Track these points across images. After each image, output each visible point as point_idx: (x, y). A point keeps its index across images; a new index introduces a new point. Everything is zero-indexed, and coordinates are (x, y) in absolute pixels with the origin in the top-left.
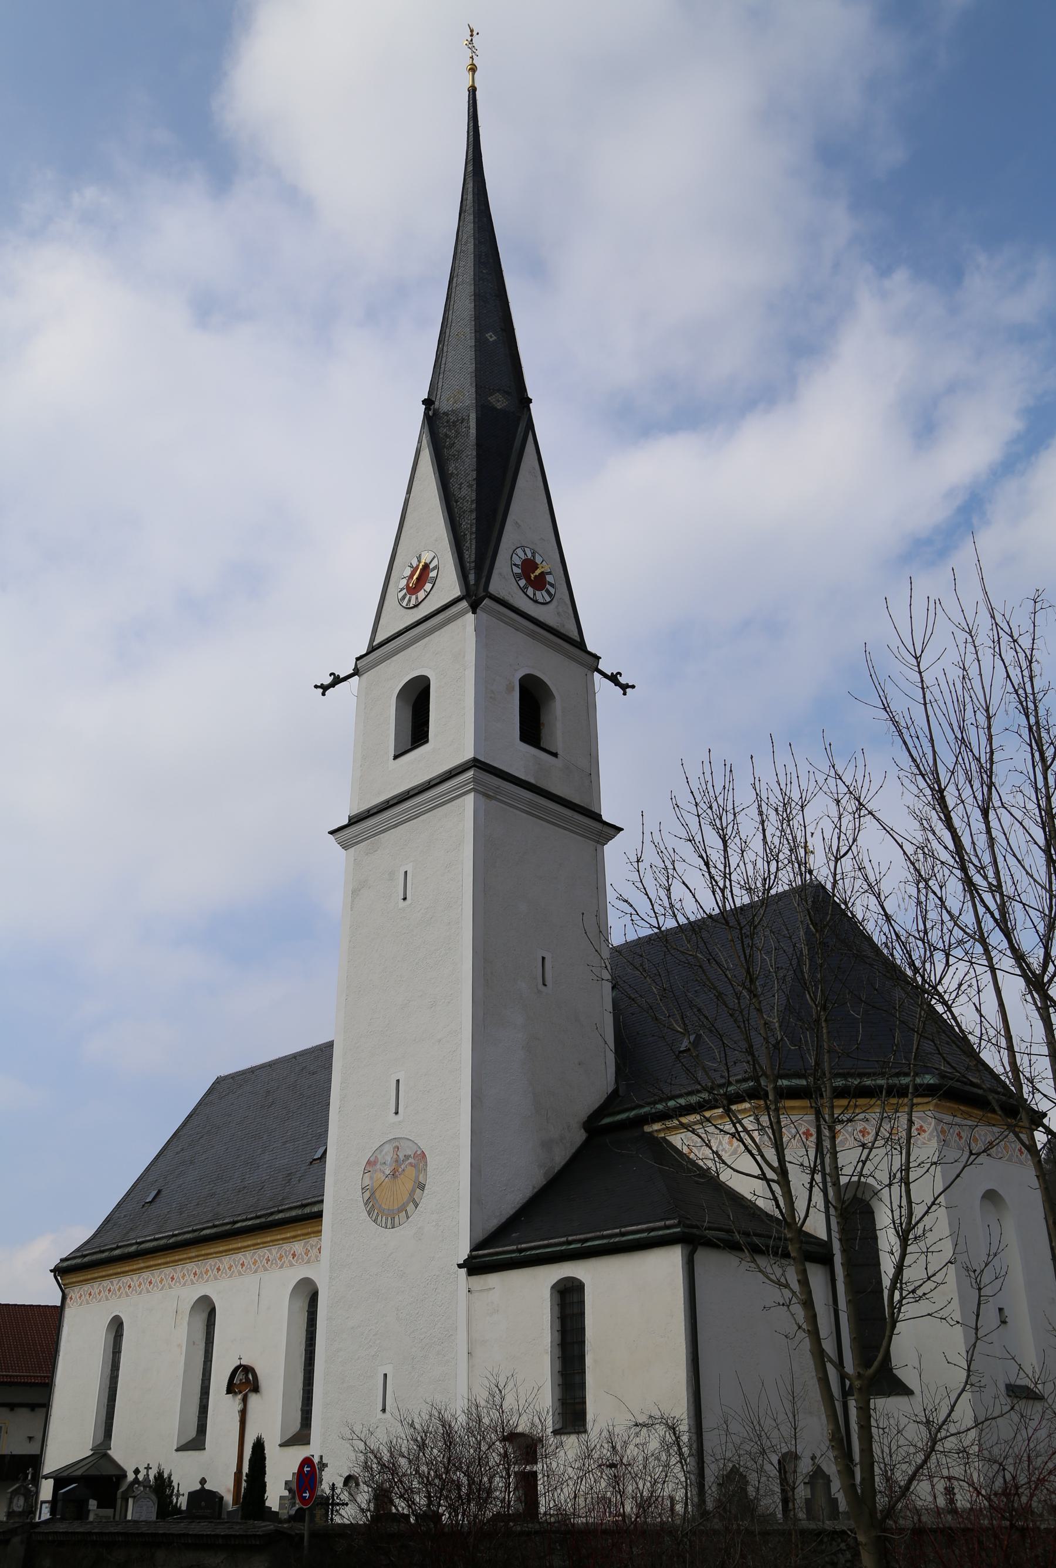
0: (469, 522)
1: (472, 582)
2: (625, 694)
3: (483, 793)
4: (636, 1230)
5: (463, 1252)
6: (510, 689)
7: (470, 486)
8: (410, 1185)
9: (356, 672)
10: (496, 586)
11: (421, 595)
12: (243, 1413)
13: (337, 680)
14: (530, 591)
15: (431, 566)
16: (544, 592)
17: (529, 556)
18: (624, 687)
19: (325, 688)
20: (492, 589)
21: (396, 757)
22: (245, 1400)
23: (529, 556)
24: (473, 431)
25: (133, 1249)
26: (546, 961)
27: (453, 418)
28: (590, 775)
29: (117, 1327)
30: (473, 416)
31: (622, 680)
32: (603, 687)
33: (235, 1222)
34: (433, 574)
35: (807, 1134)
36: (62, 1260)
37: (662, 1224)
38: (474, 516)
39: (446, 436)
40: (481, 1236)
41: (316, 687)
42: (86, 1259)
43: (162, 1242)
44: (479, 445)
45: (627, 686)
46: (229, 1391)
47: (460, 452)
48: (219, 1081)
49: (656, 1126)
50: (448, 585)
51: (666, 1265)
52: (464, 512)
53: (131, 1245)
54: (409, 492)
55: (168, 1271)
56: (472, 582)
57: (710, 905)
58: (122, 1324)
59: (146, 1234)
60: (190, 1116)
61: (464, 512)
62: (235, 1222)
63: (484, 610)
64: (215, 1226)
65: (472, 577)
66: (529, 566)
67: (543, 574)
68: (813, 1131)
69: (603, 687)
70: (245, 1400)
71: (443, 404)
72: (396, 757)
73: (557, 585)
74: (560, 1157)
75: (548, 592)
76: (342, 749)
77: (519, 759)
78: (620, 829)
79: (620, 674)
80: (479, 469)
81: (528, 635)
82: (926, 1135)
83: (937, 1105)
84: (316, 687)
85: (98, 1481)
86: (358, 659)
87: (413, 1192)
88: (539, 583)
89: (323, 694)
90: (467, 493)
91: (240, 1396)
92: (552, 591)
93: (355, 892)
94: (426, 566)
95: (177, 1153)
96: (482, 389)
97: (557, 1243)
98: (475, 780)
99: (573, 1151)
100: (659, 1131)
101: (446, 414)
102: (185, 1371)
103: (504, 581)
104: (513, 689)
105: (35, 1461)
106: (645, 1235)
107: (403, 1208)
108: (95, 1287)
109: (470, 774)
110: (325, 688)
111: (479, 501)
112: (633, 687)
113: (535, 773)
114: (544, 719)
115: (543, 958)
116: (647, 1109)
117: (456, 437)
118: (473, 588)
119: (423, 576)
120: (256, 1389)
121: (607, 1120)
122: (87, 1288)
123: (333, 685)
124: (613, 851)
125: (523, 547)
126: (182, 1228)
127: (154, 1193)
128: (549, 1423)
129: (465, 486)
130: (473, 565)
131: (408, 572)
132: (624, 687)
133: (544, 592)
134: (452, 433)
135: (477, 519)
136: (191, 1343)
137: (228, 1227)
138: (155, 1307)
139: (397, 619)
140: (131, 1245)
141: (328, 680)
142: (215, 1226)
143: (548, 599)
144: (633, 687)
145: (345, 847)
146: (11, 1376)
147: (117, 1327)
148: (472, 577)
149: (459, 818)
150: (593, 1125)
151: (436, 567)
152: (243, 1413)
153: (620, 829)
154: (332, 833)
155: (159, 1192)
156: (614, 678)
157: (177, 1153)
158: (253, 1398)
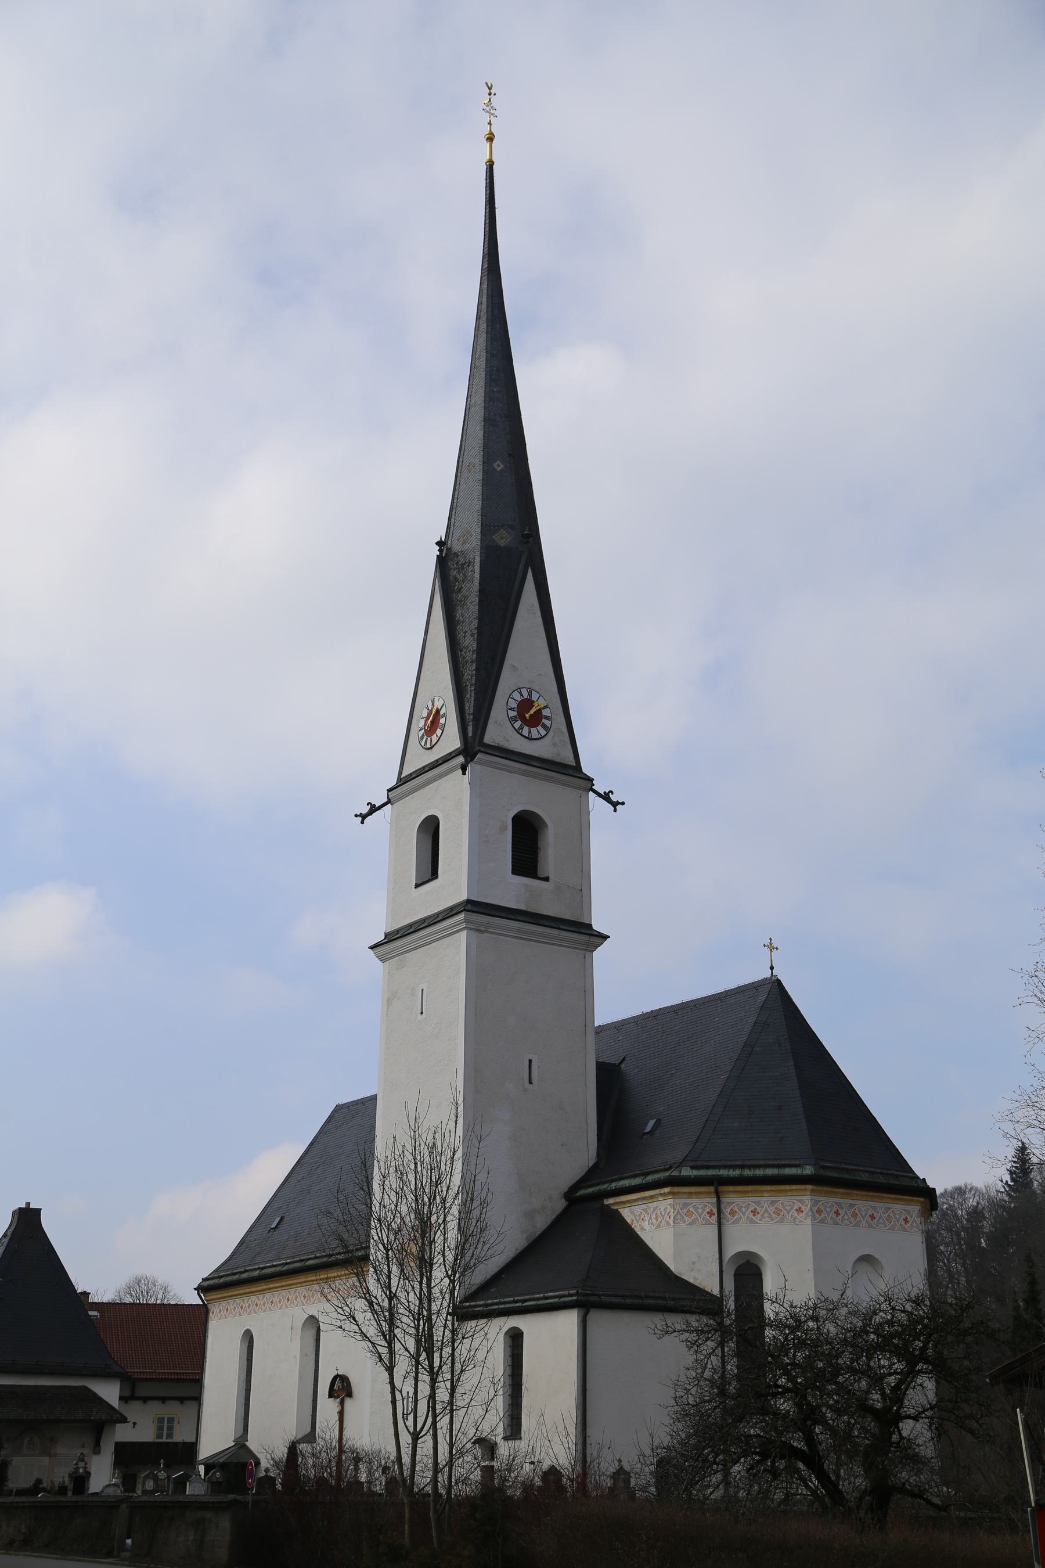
0: (469, 672)
1: (470, 734)
2: (615, 811)
3: (474, 929)
4: (553, 1296)
6: (503, 829)
7: (472, 635)
9: (389, 802)
10: (491, 736)
11: (434, 738)
12: (341, 1414)
13: (373, 809)
14: (525, 731)
15: (442, 713)
16: (540, 728)
17: (526, 695)
18: (615, 804)
19: (364, 817)
20: (488, 739)
21: (417, 886)
22: (342, 1403)
23: (526, 695)
24: (477, 576)
25: (256, 1273)
26: (533, 1063)
27: (462, 560)
28: (581, 890)
29: (248, 1338)
30: (478, 559)
31: (614, 798)
32: (596, 805)
33: (330, 1256)
34: (442, 721)
35: (711, 1214)
36: (204, 1280)
37: (566, 1292)
38: (474, 667)
39: (456, 578)
41: (356, 816)
42: (222, 1280)
43: (278, 1269)
44: (481, 591)
45: (618, 803)
46: (330, 1396)
48: (338, 1109)
49: (611, 1201)
50: (450, 739)
51: (568, 1322)
52: (467, 662)
53: (255, 1269)
54: (426, 633)
55: (284, 1293)
56: (470, 734)
58: (252, 1337)
59: (270, 1261)
60: (312, 1144)
61: (467, 662)
63: (477, 763)
64: (316, 1258)
65: (470, 729)
66: (525, 705)
67: (539, 711)
68: (715, 1211)
69: (596, 805)
70: (342, 1403)
71: (456, 546)
72: (417, 886)
73: (554, 717)
74: (542, 1223)
75: (544, 726)
76: (372, 883)
77: (512, 890)
78: (606, 937)
79: (611, 792)
80: (480, 618)
81: (522, 774)
82: (803, 1215)
83: (812, 1190)
84: (356, 816)
85: (236, 1465)
86: (389, 790)
88: (536, 720)
89: (362, 822)
90: (469, 642)
91: (338, 1400)
92: (548, 723)
93: (389, 1002)
94: (438, 711)
95: (299, 1181)
96: (487, 527)
97: (508, 1301)
98: (466, 921)
99: (554, 1217)
100: (614, 1204)
101: (456, 555)
102: (300, 1378)
103: (500, 729)
104: (506, 829)
105: (192, 1448)
106: (556, 1300)
108: (231, 1304)
109: (462, 916)
110: (364, 817)
111: (479, 651)
112: (623, 803)
114: (540, 844)
115: (530, 1061)
116: (605, 1186)
117: (463, 581)
118: (470, 740)
119: (434, 722)
120: (350, 1395)
122: (224, 1304)
123: (370, 813)
124: (600, 955)
125: (519, 690)
126: (294, 1257)
127: (278, 1220)
128: (500, 1429)
129: (468, 634)
130: (471, 717)
131: (425, 714)
132: (615, 804)
133: (540, 728)
134: (460, 577)
135: (477, 669)
136: (304, 1354)
137: (325, 1259)
138: (276, 1321)
139: (419, 759)
140: (255, 1269)
141: (365, 809)
142: (316, 1258)
143: (543, 732)
144: (623, 803)
145: (383, 960)
147: (248, 1338)
148: (470, 729)
149: (452, 953)
150: (571, 1196)
151: (445, 715)
152: (341, 1414)
153: (606, 937)
154: (371, 948)
155: (282, 1219)
156: (606, 797)
157: (299, 1181)
158: (348, 1402)
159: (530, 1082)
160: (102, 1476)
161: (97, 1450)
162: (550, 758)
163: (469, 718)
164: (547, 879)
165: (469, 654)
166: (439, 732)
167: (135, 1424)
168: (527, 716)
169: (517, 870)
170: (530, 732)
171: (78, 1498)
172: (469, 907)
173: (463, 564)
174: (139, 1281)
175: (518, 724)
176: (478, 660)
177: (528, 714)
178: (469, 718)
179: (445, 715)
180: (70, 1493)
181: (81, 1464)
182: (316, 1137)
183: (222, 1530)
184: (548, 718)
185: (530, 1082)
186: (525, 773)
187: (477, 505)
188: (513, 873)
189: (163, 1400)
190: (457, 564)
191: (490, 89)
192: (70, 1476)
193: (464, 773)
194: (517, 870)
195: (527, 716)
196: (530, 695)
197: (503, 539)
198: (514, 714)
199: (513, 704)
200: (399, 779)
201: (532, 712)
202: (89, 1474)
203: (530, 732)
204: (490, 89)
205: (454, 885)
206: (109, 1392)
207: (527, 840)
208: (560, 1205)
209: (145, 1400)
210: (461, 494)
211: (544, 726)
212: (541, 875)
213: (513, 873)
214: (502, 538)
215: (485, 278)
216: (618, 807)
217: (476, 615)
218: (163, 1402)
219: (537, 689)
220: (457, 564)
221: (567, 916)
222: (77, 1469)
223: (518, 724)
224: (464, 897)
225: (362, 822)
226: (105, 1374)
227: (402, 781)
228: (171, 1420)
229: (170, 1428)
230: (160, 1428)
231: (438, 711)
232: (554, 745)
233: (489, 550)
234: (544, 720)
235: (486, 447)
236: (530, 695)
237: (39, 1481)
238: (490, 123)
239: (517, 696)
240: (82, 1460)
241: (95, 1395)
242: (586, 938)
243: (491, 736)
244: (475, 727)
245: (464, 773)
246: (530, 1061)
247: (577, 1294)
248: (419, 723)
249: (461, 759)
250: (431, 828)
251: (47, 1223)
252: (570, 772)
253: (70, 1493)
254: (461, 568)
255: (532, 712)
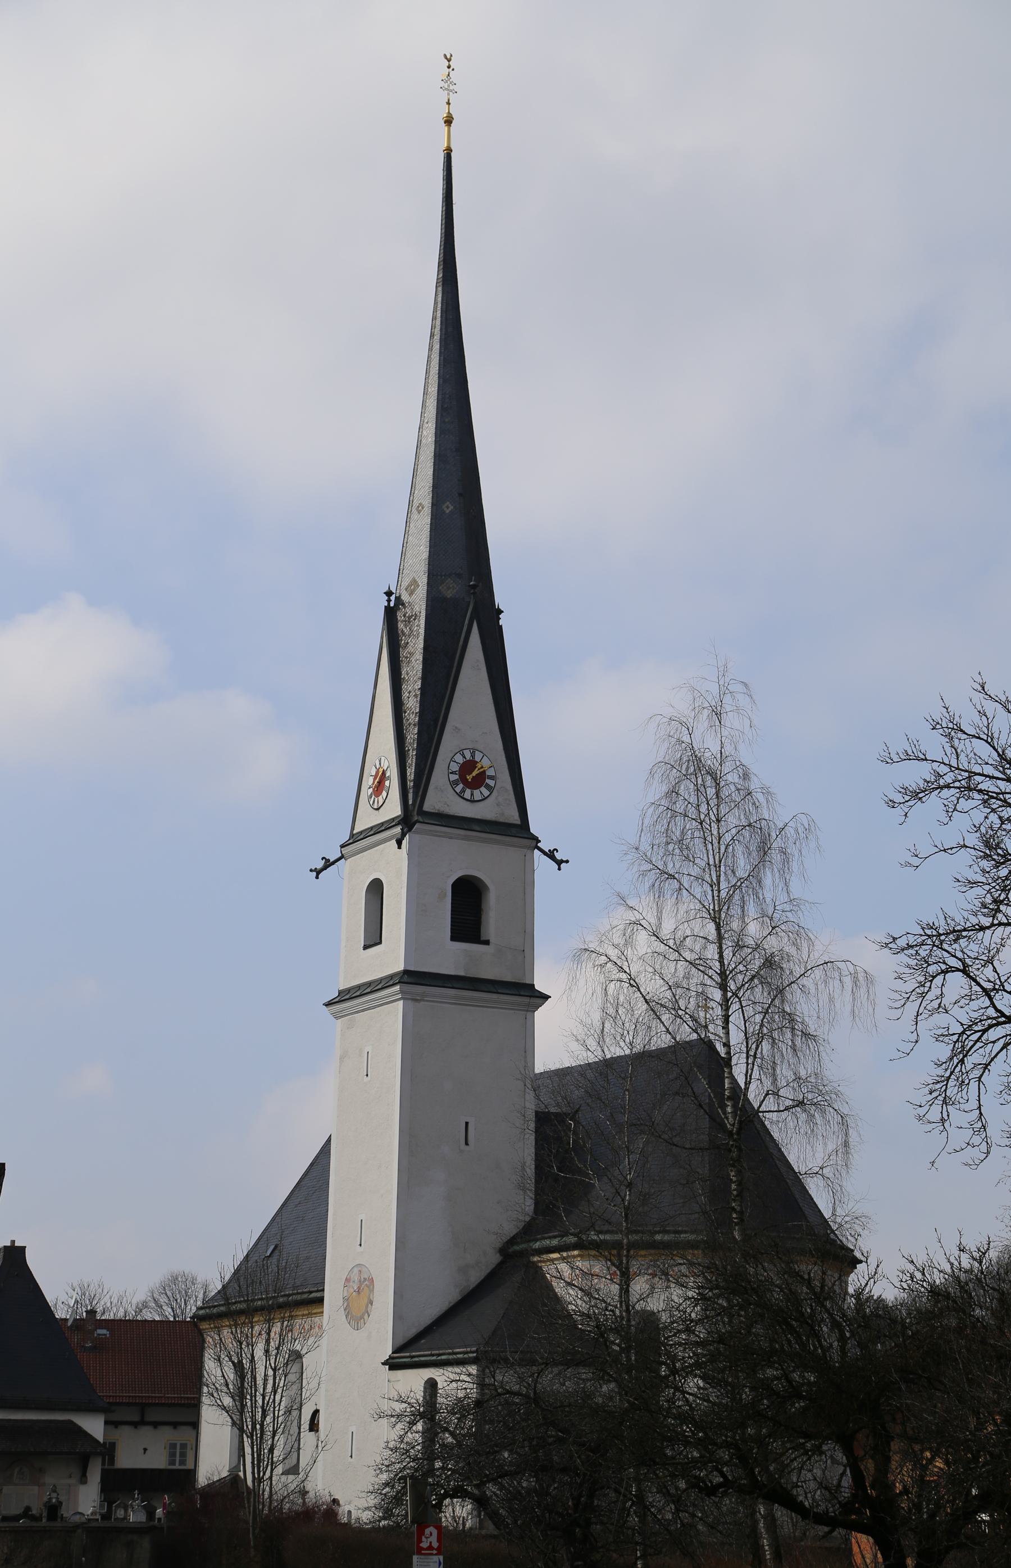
1: (410, 802)
2: (559, 869)
5: (388, 1351)
6: (442, 896)
7: (416, 696)
8: (366, 1301)
10: (430, 804)
11: (381, 800)
13: (328, 864)
14: (467, 794)
16: (483, 789)
17: (468, 756)
20: (427, 807)
21: (366, 947)
23: (468, 756)
24: (422, 631)
31: (558, 856)
32: (541, 863)
33: (311, 1292)
34: (387, 783)
38: (416, 731)
40: (401, 1342)
41: (311, 870)
45: (562, 861)
47: (412, 654)
49: (536, 1259)
50: (393, 809)
52: (410, 724)
56: (410, 802)
57: (628, 1052)
60: (312, 1165)
61: (410, 724)
62: (311, 1292)
65: (411, 796)
66: (469, 765)
69: (541, 863)
72: (366, 947)
74: (475, 1277)
75: (488, 787)
77: (451, 957)
78: (546, 997)
80: (424, 678)
81: (463, 839)
84: (311, 870)
86: (342, 846)
87: (367, 1306)
88: (479, 781)
89: (317, 877)
92: (491, 783)
95: (296, 1206)
98: (401, 991)
99: (488, 1271)
100: (540, 1261)
103: (442, 796)
104: (445, 895)
105: (191, 1474)
107: (362, 1317)
109: (397, 988)
110: (318, 872)
111: (422, 714)
112: (567, 862)
113: (469, 958)
114: (483, 906)
115: (467, 1124)
117: (409, 636)
121: (516, 1248)
123: (325, 868)
124: (542, 1015)
132: (559, 863)
134: (406, 631)
135: (419, 733)
139: (368, 819)
141: (320, 864)
143: (486, 793)
144: (567, 862)
146: (188, 1398)
148: (411, 796)
149: (388, 1020)
153: (546, 997)
154: (328, 1004)
155: (276, 1247)
156: (551, 855)
159: (467, 1144)
160: (86, 1501)
161: (83, 1479)
162: (493, 819)
163: (410, 784)
164: (487, 943)
165: (412, 716)
166: (384, 794)
167: (145, 1450)
168: (469, 778)
169: (457, 935)
170: (472, 794)
171: (52, 1524)
172: (406, 978)
173: (410, 617)
174: (175, 1279)
175: (459, 788)
176: (421, 724)
177: (470, 775)
178: (410, 784)
179: (389, 778)
180: (44, 1520)
181: (54, 1495)
182: (317, 1157)
183: (144, 1548)
184: (492, 778)
185: (467, 1144)
186: (466, 838)
187: (425, 555)
188: (453, 938)
189: (175, 1425)
190: (404, 616)
191: (449, 60)
192: (45, 1505)
193: (399, 847)
194: (457, 935)
195: (469, 778)
196: (473, 755)
197: (451, 589)
198: (456, 777)
199: (455, 767)
200: (352, 835)
201: (474, 774)
202: (61, 1503)
203: (472, 794)
204: (449, 60)
205: (391, 957)
206: (94, 1426)
207: (468, 908)
208: (495, 1259)
209: (156, 1425)
210: (410, 538)
211: (488, 787)
212: (483, 938)
213: (453, 938)
214: (449, 588)
215: (440, 289)
216: (563, 865)
217: (420, 674)
218: (175, 1428)
219: (480, 748)
220: (404, 616)
221: (508, 978)
222: (50, 1499)
223: (459, 788)
224: (400, 967)
225: (317, 877)
226: (90, 1408)
227: (355, 837)
228: (184, 1446)
229: (183, 1455)
230: (172, 1455)
231: (384, 773)
232: (498, 805)
233: (434, 601)
234: (488, 781)
235: (436, 487)
236: (473, 755)
237: (28, 1509)
238: (448, 103)
239: (459, 759)
240: (55, 1491)
241: (80, 1428)
242: (527, 1000)
243: (430, 804)
244: (415, 794)
245: (399, 847)
246: (467, 1124)
247: (476, 1351)
248: (369, 781)
249: (398, 830)
250: (376, 888)
251: (32, 1261)
252: (518, 831)
253: (44, 1520)
254: (408, 621)
255: (474, 774)
